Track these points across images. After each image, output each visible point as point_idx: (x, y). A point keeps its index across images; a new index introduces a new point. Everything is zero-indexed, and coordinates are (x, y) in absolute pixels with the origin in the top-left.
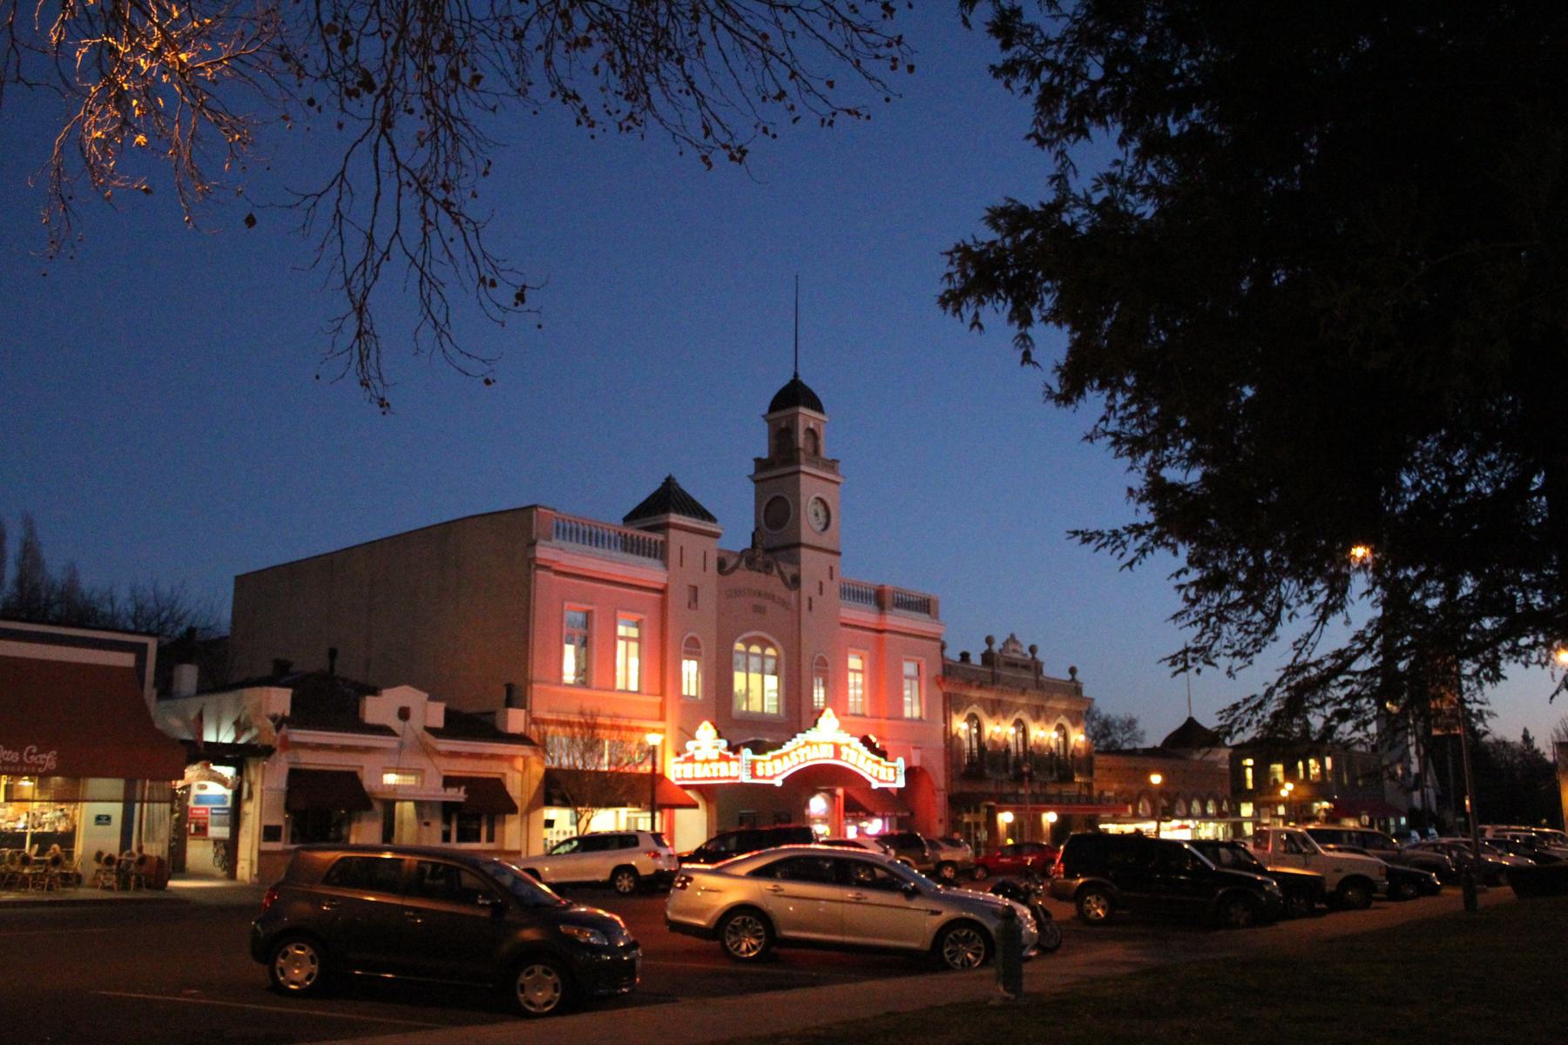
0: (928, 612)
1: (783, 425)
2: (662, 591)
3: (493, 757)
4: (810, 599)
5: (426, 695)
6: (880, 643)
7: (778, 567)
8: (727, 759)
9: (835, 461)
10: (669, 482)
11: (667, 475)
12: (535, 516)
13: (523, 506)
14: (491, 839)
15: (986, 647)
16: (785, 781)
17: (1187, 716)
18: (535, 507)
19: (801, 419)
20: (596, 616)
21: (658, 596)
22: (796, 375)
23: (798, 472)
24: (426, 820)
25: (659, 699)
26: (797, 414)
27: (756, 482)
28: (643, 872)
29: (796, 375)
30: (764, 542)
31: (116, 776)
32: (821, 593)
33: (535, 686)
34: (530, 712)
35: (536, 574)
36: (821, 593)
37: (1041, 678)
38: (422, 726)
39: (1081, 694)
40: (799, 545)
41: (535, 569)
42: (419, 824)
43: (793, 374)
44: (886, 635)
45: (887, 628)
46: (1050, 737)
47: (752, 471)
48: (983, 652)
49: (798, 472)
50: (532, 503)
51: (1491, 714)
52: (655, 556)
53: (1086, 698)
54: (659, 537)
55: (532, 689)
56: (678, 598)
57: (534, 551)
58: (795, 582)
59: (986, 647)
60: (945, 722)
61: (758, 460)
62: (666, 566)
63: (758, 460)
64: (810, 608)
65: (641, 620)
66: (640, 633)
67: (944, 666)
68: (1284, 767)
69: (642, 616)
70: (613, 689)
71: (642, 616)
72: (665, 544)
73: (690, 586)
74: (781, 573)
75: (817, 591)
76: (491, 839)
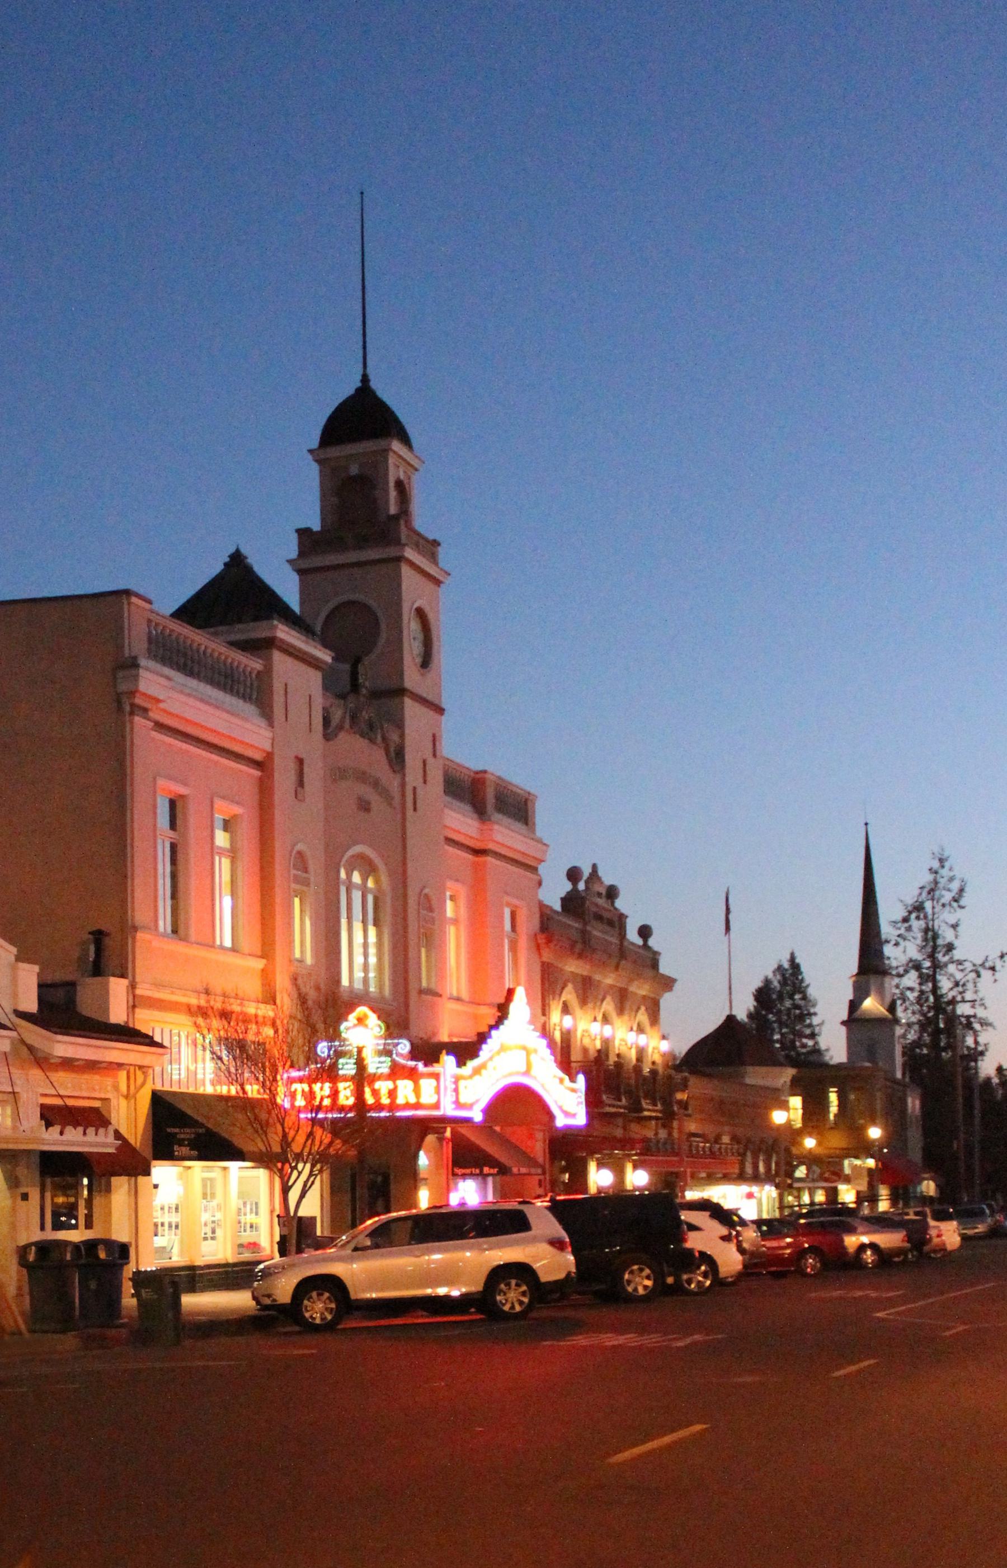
0: (527, 824)
1: (354, 470)
2: (263, 765)
3: (92, 1066)
4: (415, 788)
5: (14, 950)
6: (477, 869)
7: (382, 728)
8: (412, 1074)
9: (436, 543)
10: (237, 560)
11: (232, 550)
12: (126, 607)
13: (96, 591)
14: (89, 1225)
15: (568, 886)
16: (487, 1111)
17: (727, 1013)
18: (127, 593)
19: (392, 460)
20: (192, 808)
21: (257, 773)
22: (365, 379)
23: (399, 559)
24: (24, 1190)
25: (260, 964)
26: (387, 451)
27: (301, 572)
28: (544, 1278)
29: (365, 379)
30: (367, 684)
31: (848, 1058)
32: (425, 782)
33: (139, 935)
34: (133, 986)
35: (132, 723)
36: (425, 782)
37: (626, 944)
38: (13, 1008)
39: (658, 969)
40: (401, 692)
41: (132, 713)
42: (13, 1197)
43: (359, 377)
44: (490, 859)
45: (491, 846)
46: (641, 1053)
47: (294, 554)
48: (563, 895)
49: (399, 559)
50: (121, 586)
51: (985, 1023)
52: (250, 699)
53: (663, 975)
54: (255, 664)
55: (134, 938)
56: (284, 780)
57: (136, 678)
58: (397, 758)
59: (568, 886)
60: (544, 1014)
61: (303, 533)
62: (271, 724)
63: (303, 533)
64: (415, 809)
65: (235, 817)
66: (232, 841)
67: (542, 915)
68: (804, 1102)
69: (238, 810)
70: (212, 946)
71: (238, 810)
72: (265, 676)
73: (297, 757)
74: (384, 739)
75: (421, 780)
76: (89, 1225)
